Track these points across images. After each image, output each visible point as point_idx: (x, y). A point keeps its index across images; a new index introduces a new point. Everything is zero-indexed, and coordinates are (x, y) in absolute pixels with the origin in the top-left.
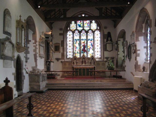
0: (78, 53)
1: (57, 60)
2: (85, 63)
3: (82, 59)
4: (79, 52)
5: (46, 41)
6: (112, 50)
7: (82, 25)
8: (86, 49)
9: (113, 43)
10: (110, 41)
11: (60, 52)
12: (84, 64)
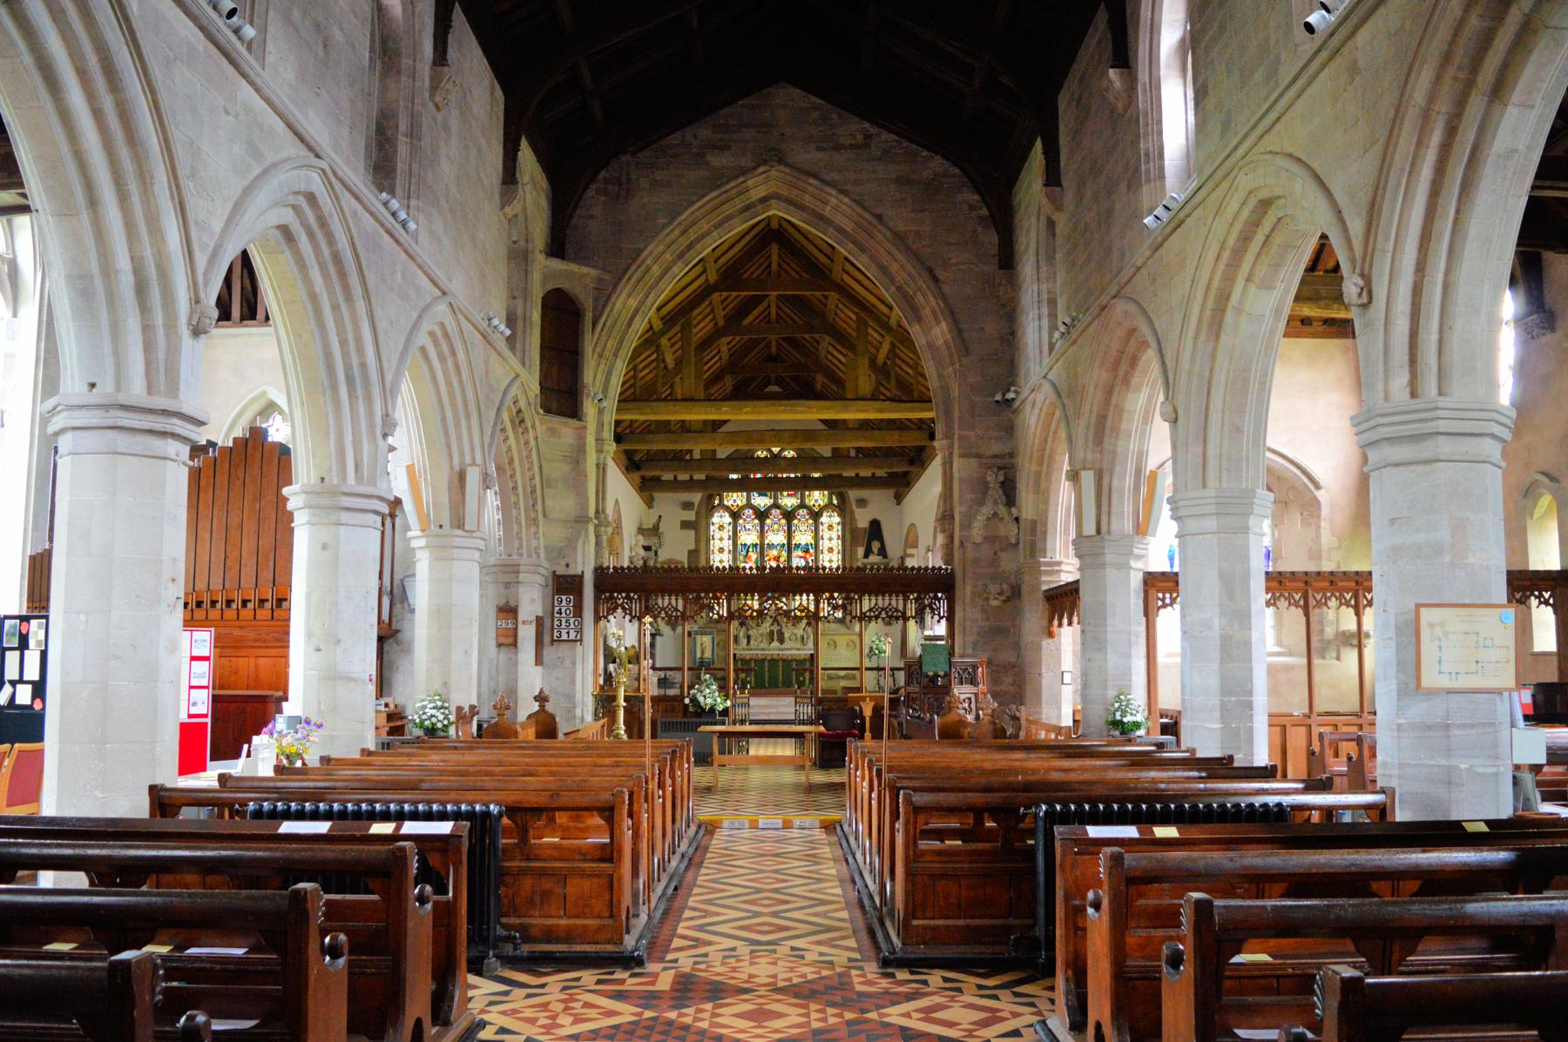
2: (781, 641)
12: (775, 644)
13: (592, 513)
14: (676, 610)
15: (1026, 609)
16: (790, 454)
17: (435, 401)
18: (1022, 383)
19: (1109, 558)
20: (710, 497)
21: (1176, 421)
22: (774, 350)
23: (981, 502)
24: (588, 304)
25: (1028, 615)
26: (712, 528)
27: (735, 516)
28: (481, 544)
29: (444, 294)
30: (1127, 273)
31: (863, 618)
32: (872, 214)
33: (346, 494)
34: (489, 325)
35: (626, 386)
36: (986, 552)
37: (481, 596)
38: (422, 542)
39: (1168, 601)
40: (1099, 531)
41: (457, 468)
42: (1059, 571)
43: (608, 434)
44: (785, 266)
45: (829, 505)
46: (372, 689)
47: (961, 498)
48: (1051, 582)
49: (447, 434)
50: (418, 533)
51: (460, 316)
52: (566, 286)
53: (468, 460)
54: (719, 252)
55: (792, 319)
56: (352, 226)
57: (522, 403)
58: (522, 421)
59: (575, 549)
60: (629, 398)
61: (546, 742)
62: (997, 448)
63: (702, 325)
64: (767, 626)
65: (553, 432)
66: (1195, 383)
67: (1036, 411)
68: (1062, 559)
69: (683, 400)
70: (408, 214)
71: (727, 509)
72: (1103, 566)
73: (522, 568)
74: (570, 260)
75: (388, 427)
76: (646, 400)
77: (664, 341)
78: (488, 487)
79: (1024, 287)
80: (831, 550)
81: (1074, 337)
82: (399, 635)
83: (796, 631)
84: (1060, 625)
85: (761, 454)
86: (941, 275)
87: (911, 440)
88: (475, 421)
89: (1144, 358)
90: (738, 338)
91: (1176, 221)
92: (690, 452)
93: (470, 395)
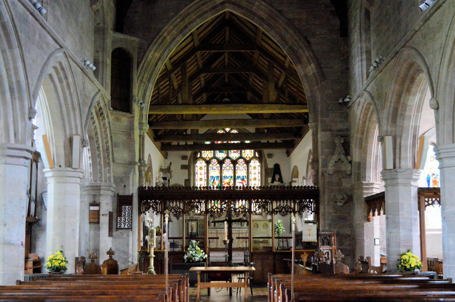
10: (279, 181)
13: (137, 160)
14: (180, 208)
15: (356, 207)
16: (235, 131)
17: (57, 102)
18: (353, 94)
19: (400, 181)
20: (196, 153)
21: (437, 109)
22: (227, 80)
23: (333, 154)
24: (135, 56)
25: (356, 211)
26: (196, 169)
27: (208, 162)
28: (81, 175)
29: (61, 47)
30: (409, 34)
31: (272, 212)
32: (276, 10)
33: (9, 148)
34: (85, 64)
35: (154, 98)
36: (335, 179)
37: (81, 202)
38: (50, 174)
39: (430, 202)
40: (395, 167)
41: (68, 137)
42: (373, 188)
43: (145, 120)
44: (232, 38)
45: (254, 157)
46: (22, 250)
47: (322, 152)
48: (368, 193)
49: (63, 120)
50: (49, 170)
51: (68, 57)
52: (124, 46)
53: (74, 132)
54: (199, 31)
55: (235, 64)
56: (12, 10)
57: (102, 105)
58: (102, 114)
59: (129, 178)
60: (153, 105)
61: (113, 276)
62: (340, 126)
63: (192, 67)
65: (118, 120)
66: (448, 89)
67: (360, 107)
68: (374, 182)
69: (182, 104)
70: (42, 6)
71: (204, 159)
72: (397, 184)
73: (102, 188)
74: (126, 33)
75: (32, 114)
76: (164, 105)
77: (173, 75)
78: (84, 146)
79: (353, 46)
80: (255, 179)
81: (381, 68)
82: (40, 222)
84: (374, 215)
85: (220, 132)
86: (312, 40)
87: (294, 124)
88: (77, 113)
89: (418, 78)
90: (210, 74)
91: (437, 6)
92: (186, 130)
93: (75, 100)
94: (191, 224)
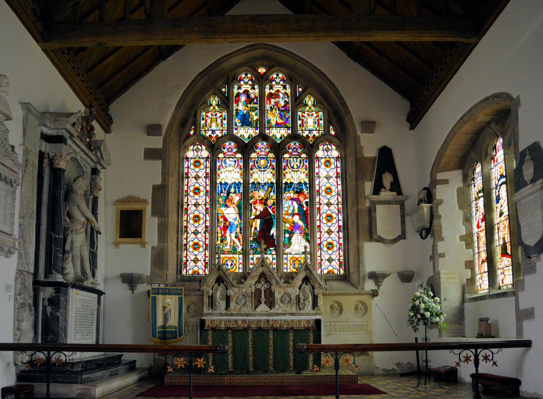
0: (234, 251)
1: (126, 286)
2: (271, 304)
3: (253, 282)
4: (240, 249)
5: (41, 155)
6: (403, 236)
7: (255, 117)
8: (273, 231)
9: (407, 203)
10: (391, 190)
11: (143, 245)
12: (263, 308)
64: (250, 286)
80: (330, 246)
83: (289, 290)
94: (164, 300)
